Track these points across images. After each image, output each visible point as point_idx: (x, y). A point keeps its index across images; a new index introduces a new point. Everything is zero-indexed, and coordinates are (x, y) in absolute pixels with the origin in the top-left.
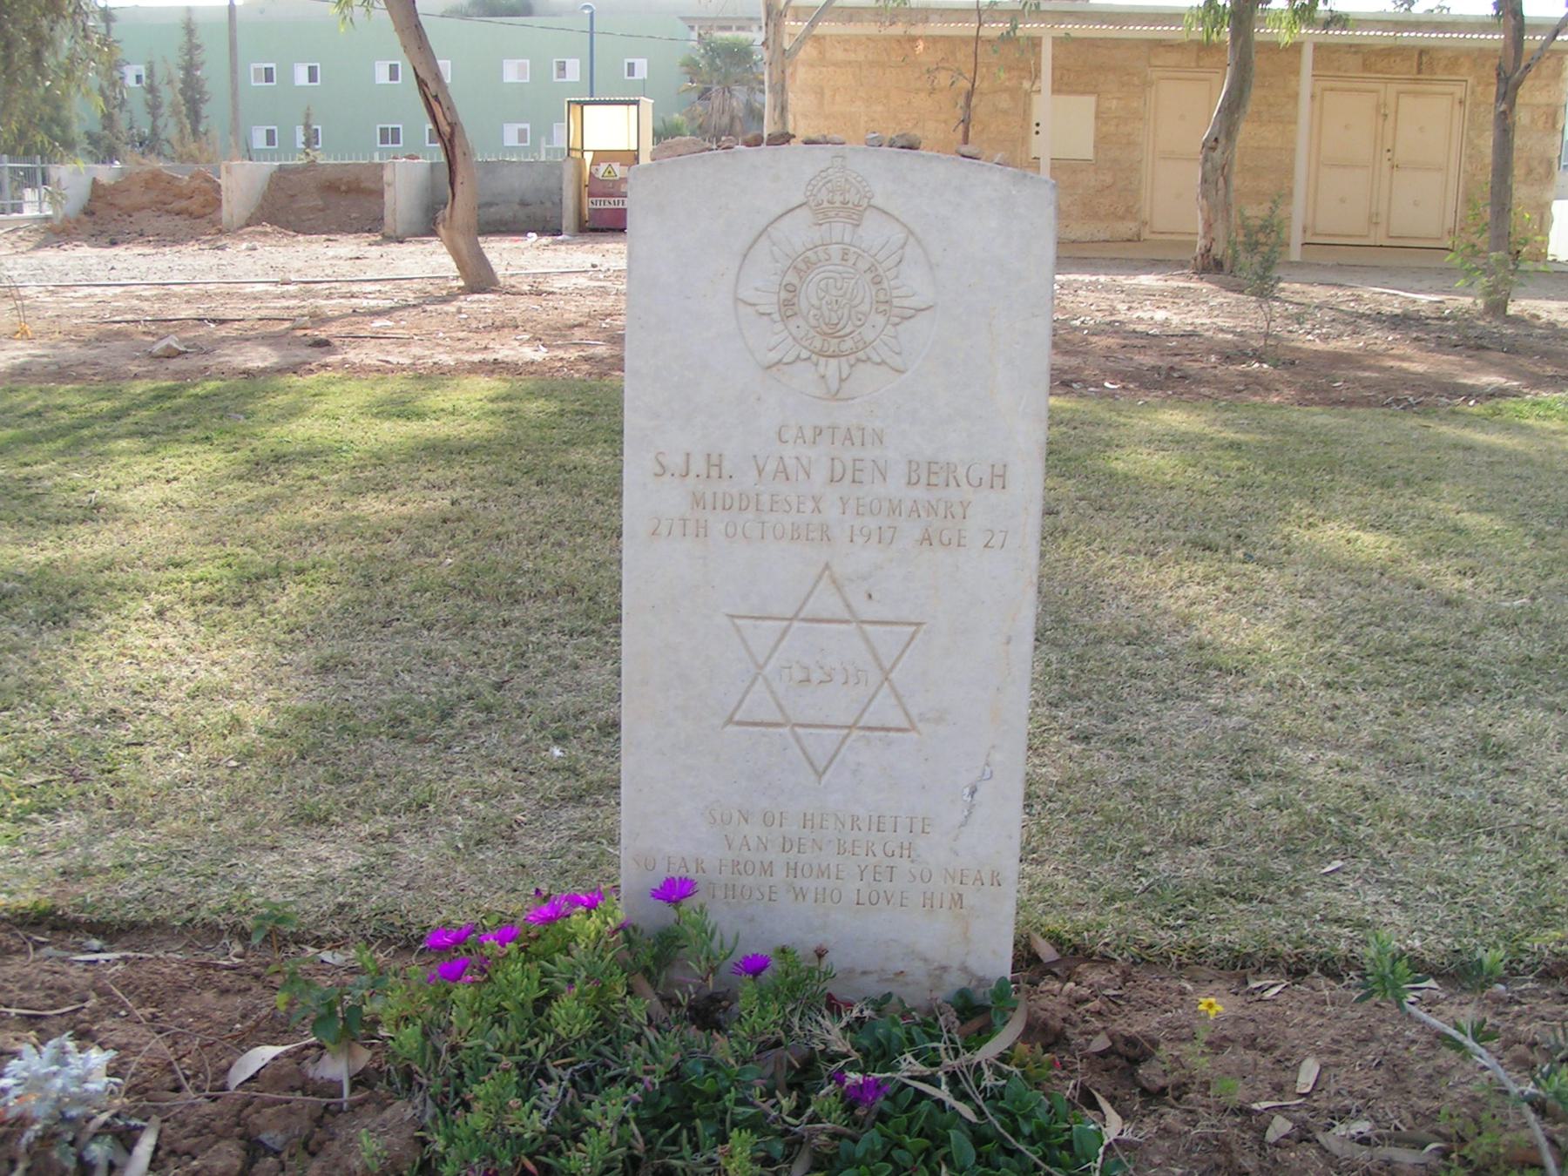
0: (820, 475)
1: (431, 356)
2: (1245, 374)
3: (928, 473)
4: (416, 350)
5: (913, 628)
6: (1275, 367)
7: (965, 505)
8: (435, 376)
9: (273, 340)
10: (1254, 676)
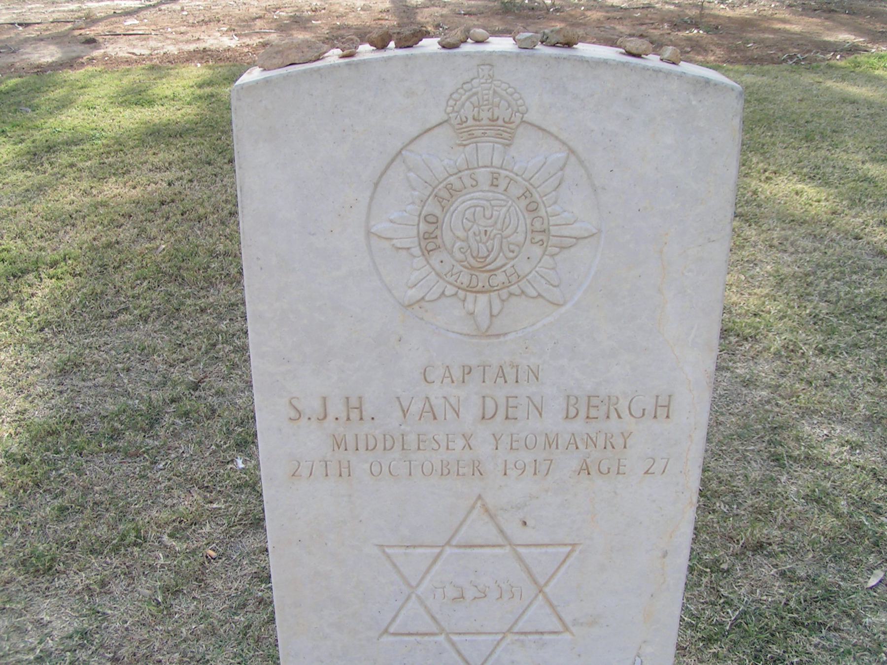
0: (471, 413)
1: (163, 47)
2: (689, 39)
3: (590, 407)
4: (152, 43)
5: (569, 548)
6: (707, 32)
7: (626, 436)
8: (161, 66)
9: (57, 39)
10: (766, 342)
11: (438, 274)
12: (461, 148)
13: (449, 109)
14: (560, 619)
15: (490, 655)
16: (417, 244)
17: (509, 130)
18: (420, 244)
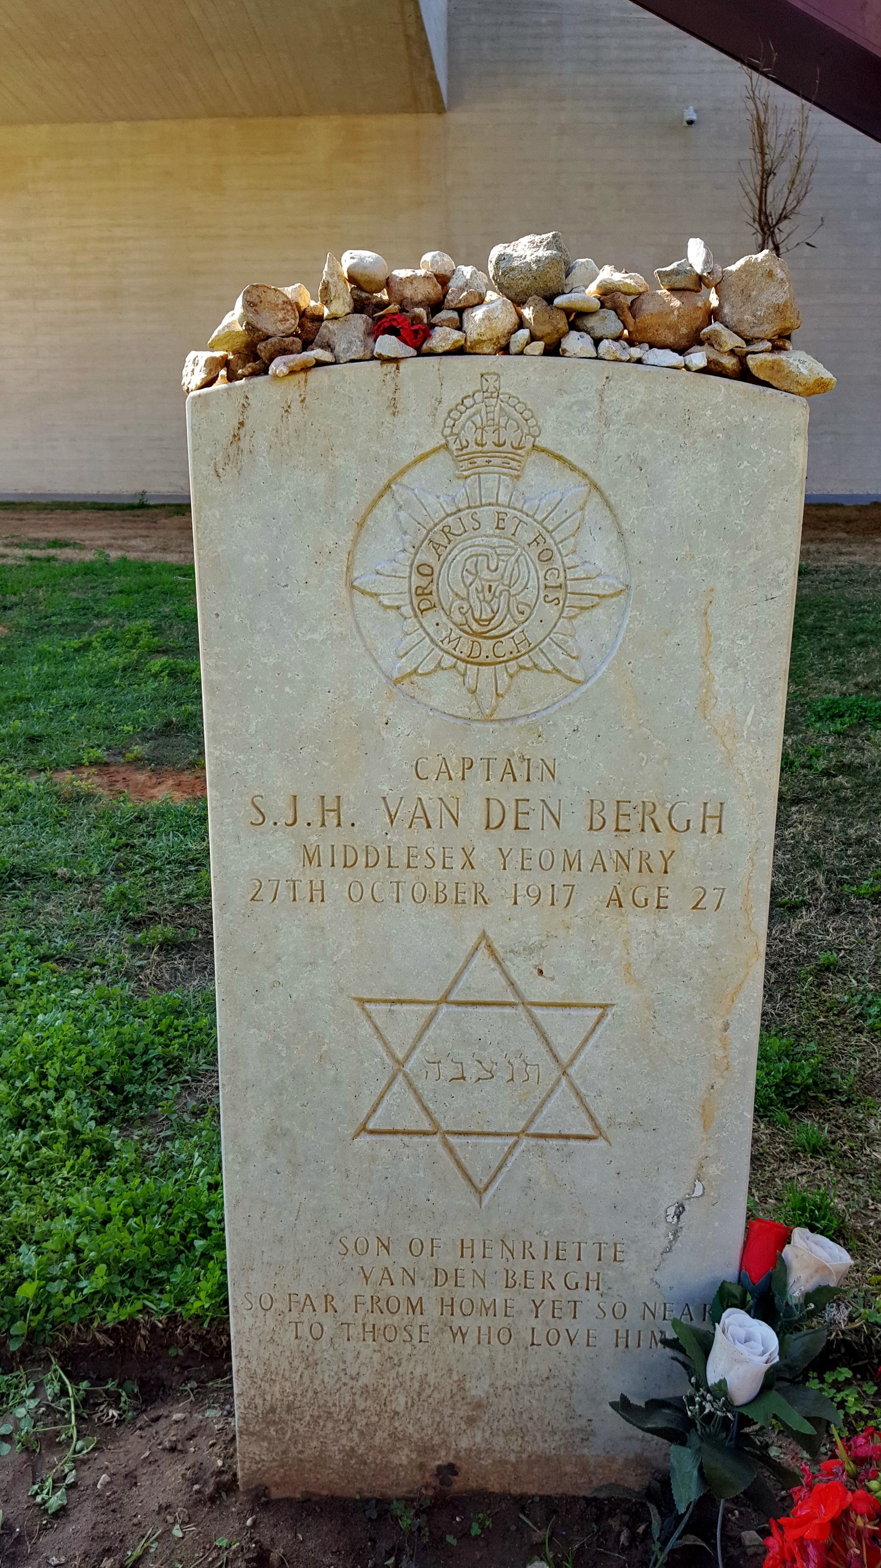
3: (623, 816)
11: (432, 640)
12: (461, 482)
13: (447, 431)
14: (592, 1118)
15: (500, 1168)
16: (408, 601)
17: (517, 458)
18: (411, 603)
